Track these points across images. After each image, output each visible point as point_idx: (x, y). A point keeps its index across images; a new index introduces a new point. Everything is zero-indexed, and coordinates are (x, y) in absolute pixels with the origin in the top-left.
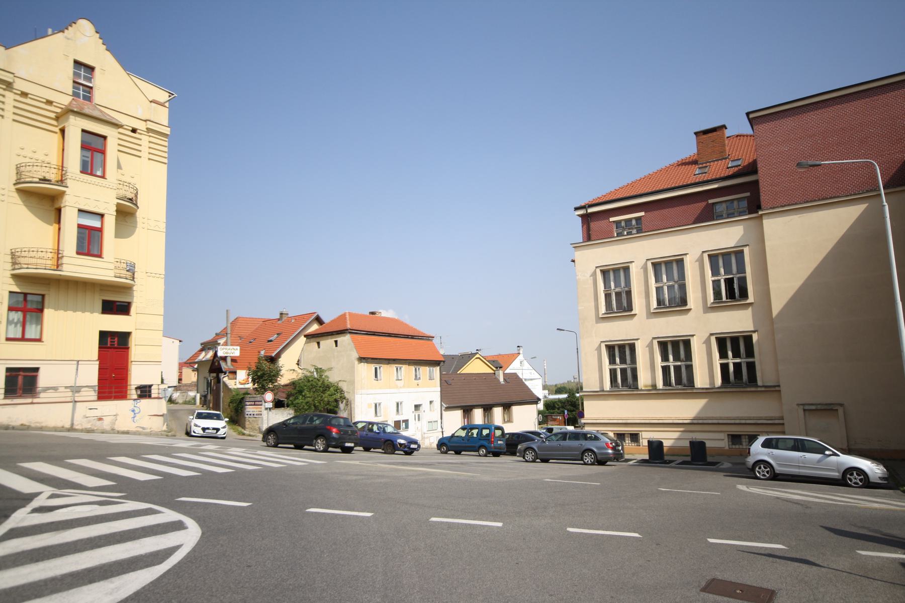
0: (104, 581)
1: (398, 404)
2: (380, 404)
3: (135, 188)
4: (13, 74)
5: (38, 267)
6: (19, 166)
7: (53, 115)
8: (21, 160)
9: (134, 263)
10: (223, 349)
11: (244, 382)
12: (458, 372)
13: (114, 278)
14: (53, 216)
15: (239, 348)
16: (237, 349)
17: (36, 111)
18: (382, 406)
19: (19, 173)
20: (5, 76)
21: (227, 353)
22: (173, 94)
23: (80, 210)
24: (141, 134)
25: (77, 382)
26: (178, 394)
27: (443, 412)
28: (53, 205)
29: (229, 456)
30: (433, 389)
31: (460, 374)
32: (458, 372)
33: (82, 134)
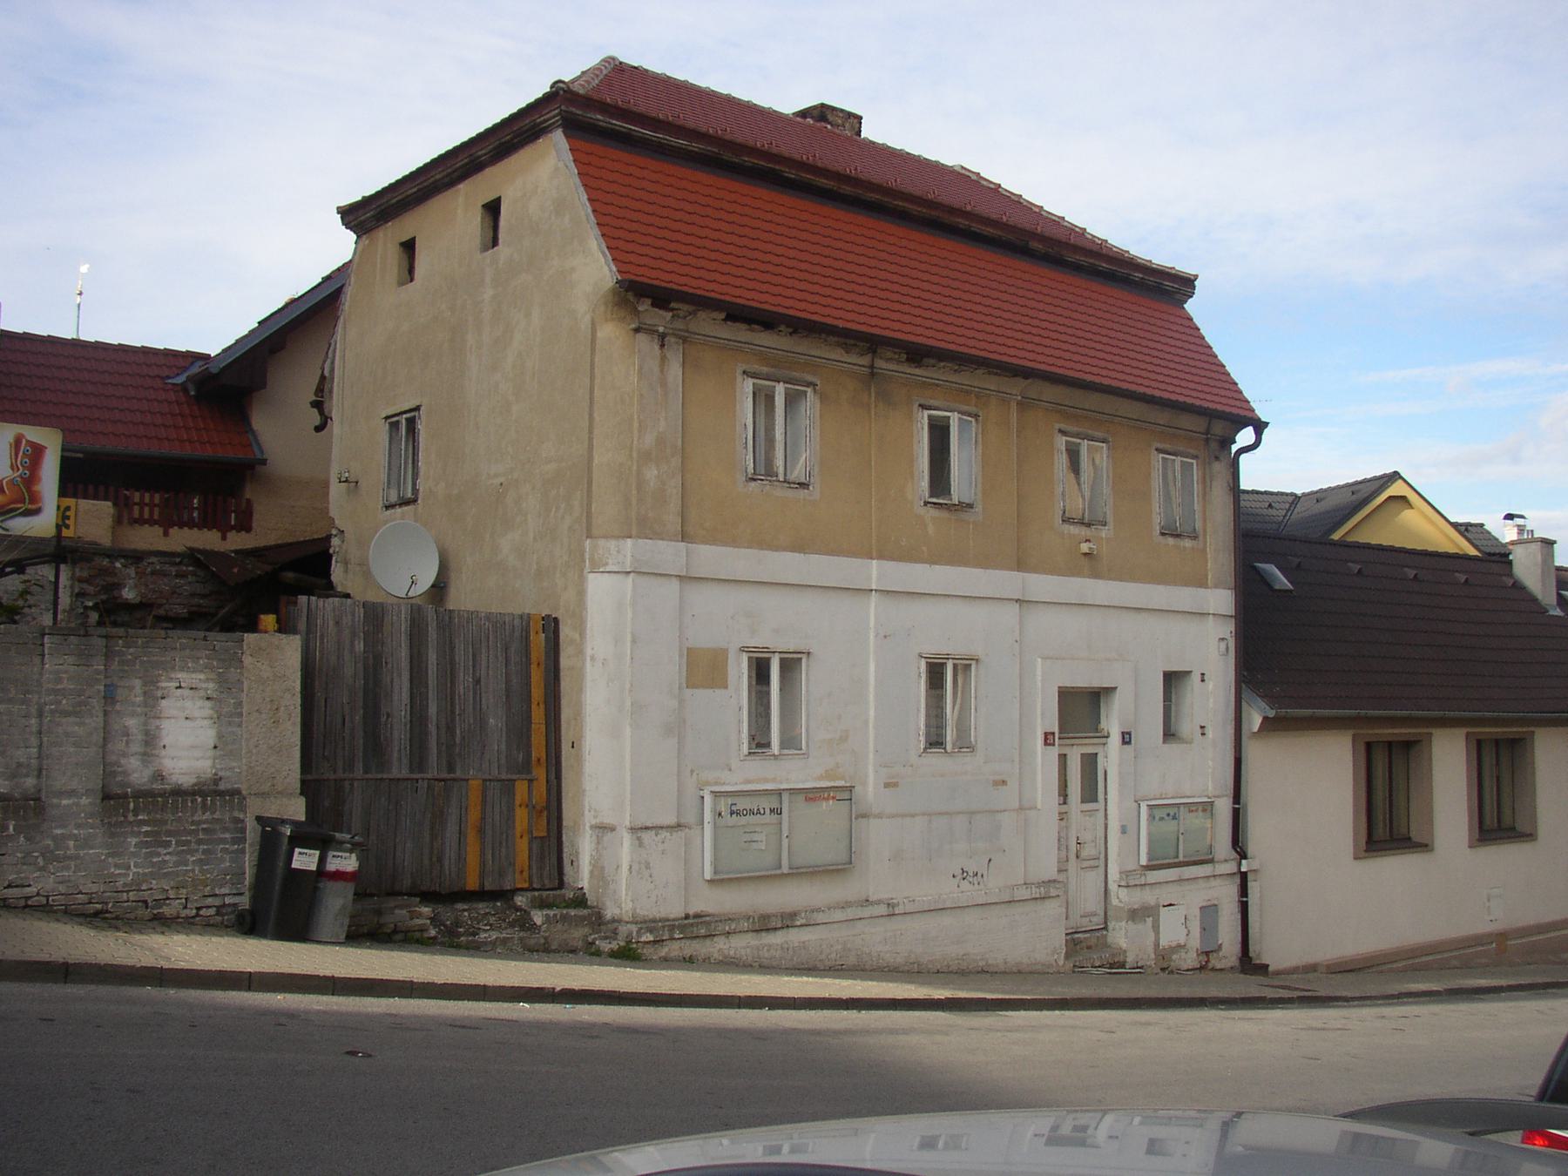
0: (1548, 729)
1: (935, 673)
2: (790, 665)
5: (726, 342)
12: (1336, 536)
18: (811, 679)
26: (134, 721)
27: (1255, 753)
29: (670, 1011)
30: (1183, 597)
31: (1342, 544)
32: (1336, 536)
33: (1431, 833)
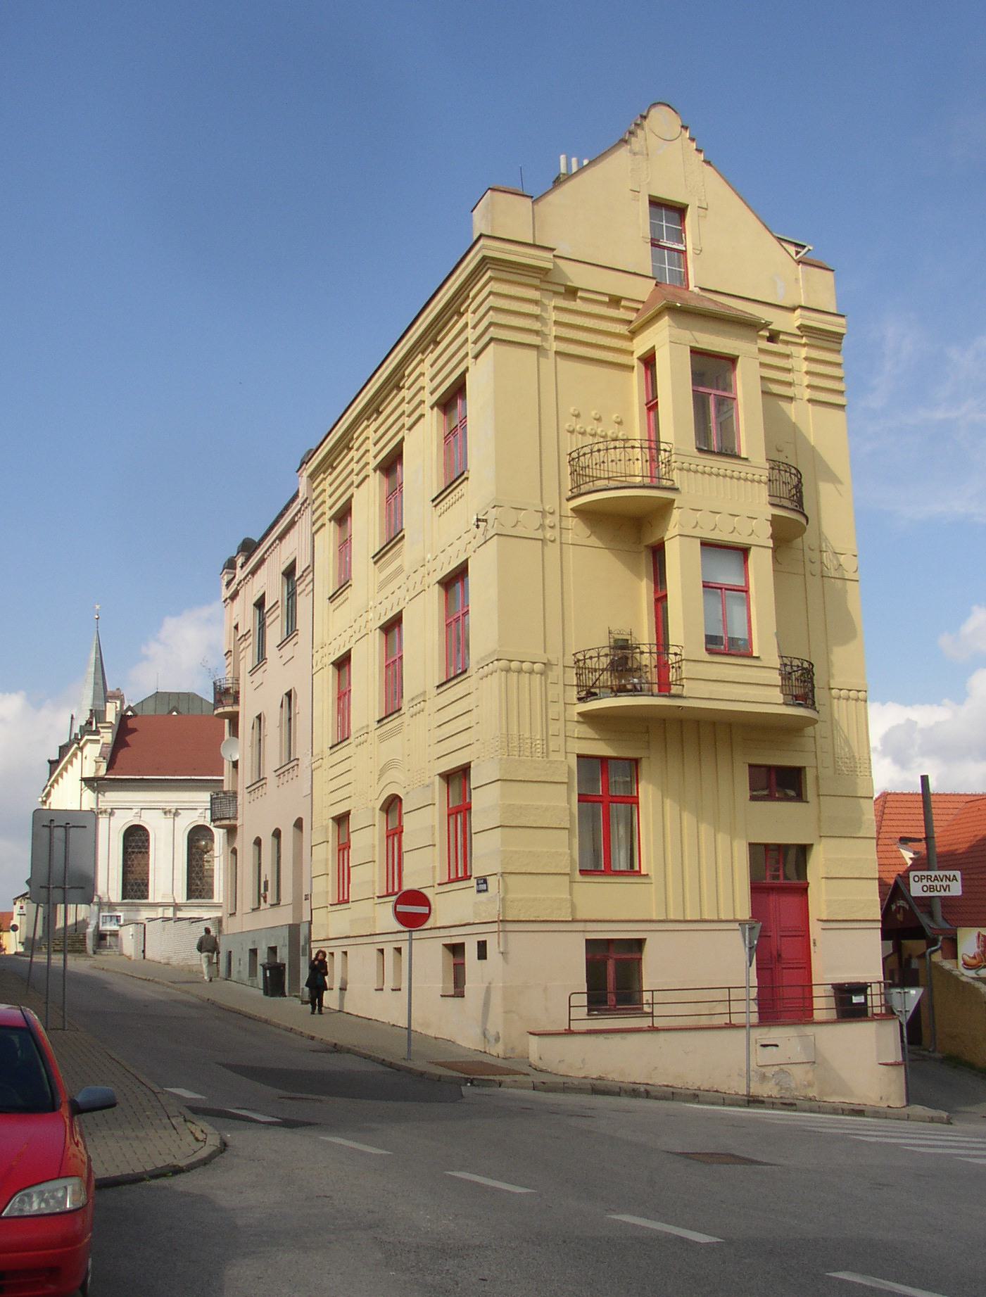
3: (793, 471)
4: (552, 250)
6: (575, 455)
7: (623, 329)
8: (571, 443)
9: (811, 664)
10: (921, 879)
11: (974, 962)
13: (784, 707)
14: (645, 562)
15: (958, 874)
16: (955, 878)
17: (443, 362)
19: (578, 473)
20: (524, 255)
21: (931, 888)
22: (804, 247)
23: (706, 545)
24: (787, 343)
25: (497, 937)
28: (639, 540)
